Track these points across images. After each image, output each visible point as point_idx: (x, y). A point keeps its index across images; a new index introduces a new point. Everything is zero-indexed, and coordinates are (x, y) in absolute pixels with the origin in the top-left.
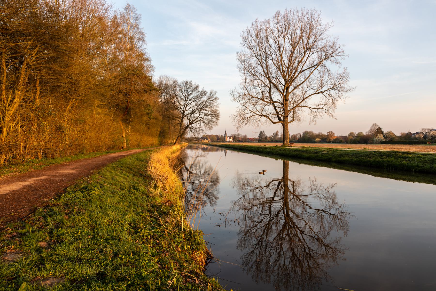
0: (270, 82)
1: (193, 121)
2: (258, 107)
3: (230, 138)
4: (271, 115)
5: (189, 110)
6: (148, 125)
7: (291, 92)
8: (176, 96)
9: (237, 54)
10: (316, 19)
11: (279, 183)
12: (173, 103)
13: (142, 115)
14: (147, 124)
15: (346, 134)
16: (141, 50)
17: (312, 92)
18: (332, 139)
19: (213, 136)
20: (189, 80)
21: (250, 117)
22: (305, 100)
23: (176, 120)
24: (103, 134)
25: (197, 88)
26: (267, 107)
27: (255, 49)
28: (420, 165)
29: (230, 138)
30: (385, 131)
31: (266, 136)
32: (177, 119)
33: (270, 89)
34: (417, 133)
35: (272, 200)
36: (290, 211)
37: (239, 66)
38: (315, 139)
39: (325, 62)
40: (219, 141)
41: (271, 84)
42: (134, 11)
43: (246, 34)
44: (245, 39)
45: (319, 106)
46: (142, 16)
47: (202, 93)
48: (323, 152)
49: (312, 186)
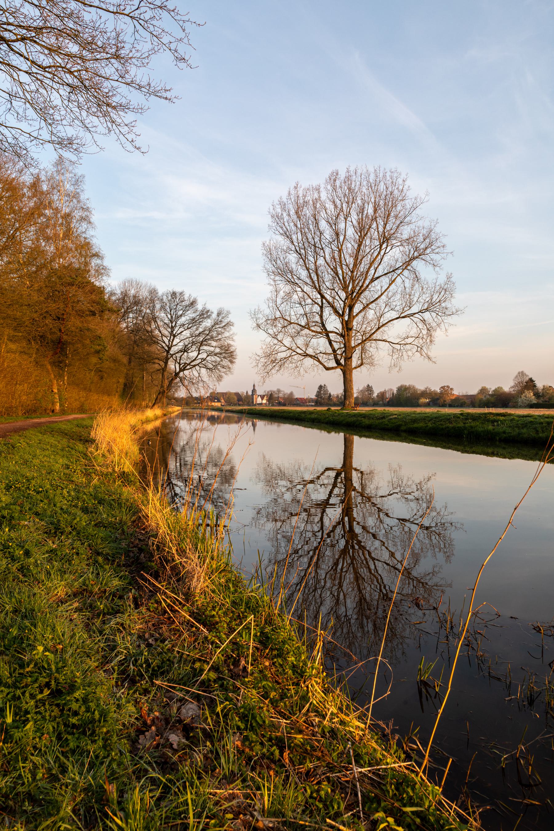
0: (323, 297)
2: (300, 341)
4: (322, 355)
5: (178, 345)
6: (101, 371)
7: (357, 315)
8: (155, 319)
9: (264, 244)
10: (401, 187)
11: (338, 475)
12: (148, 332)
13: (88, 354)
14: (99, 371)
15: (474, 391)
16: (85, 238)
17: (394, 315)
18: (448, 399)
19: (230, 394)
20: (178, 290)
21: (285, 358)
22: (381, 329)
23: (154, 363)
24: (18, 386)
25: (193, 304)
26: (314, 341)
27: (294, 237)
28: (508, 430)
30: (540, 385)
31: (330, 394)
32: (157, 361)
33: (321, 307)
35: (325, 505)
36: (355, 523)
37: (267, 266)
38: (418, 399)
39: (414, 263)
40: (241, 403)
41: (324, 301)
42: (71, 168)
43: (279, 210)
44: (277, 218)
45: (406, 340)
46: (86, 179)
47: (203, 314)
48: (392, 417)
49: (395, 479)
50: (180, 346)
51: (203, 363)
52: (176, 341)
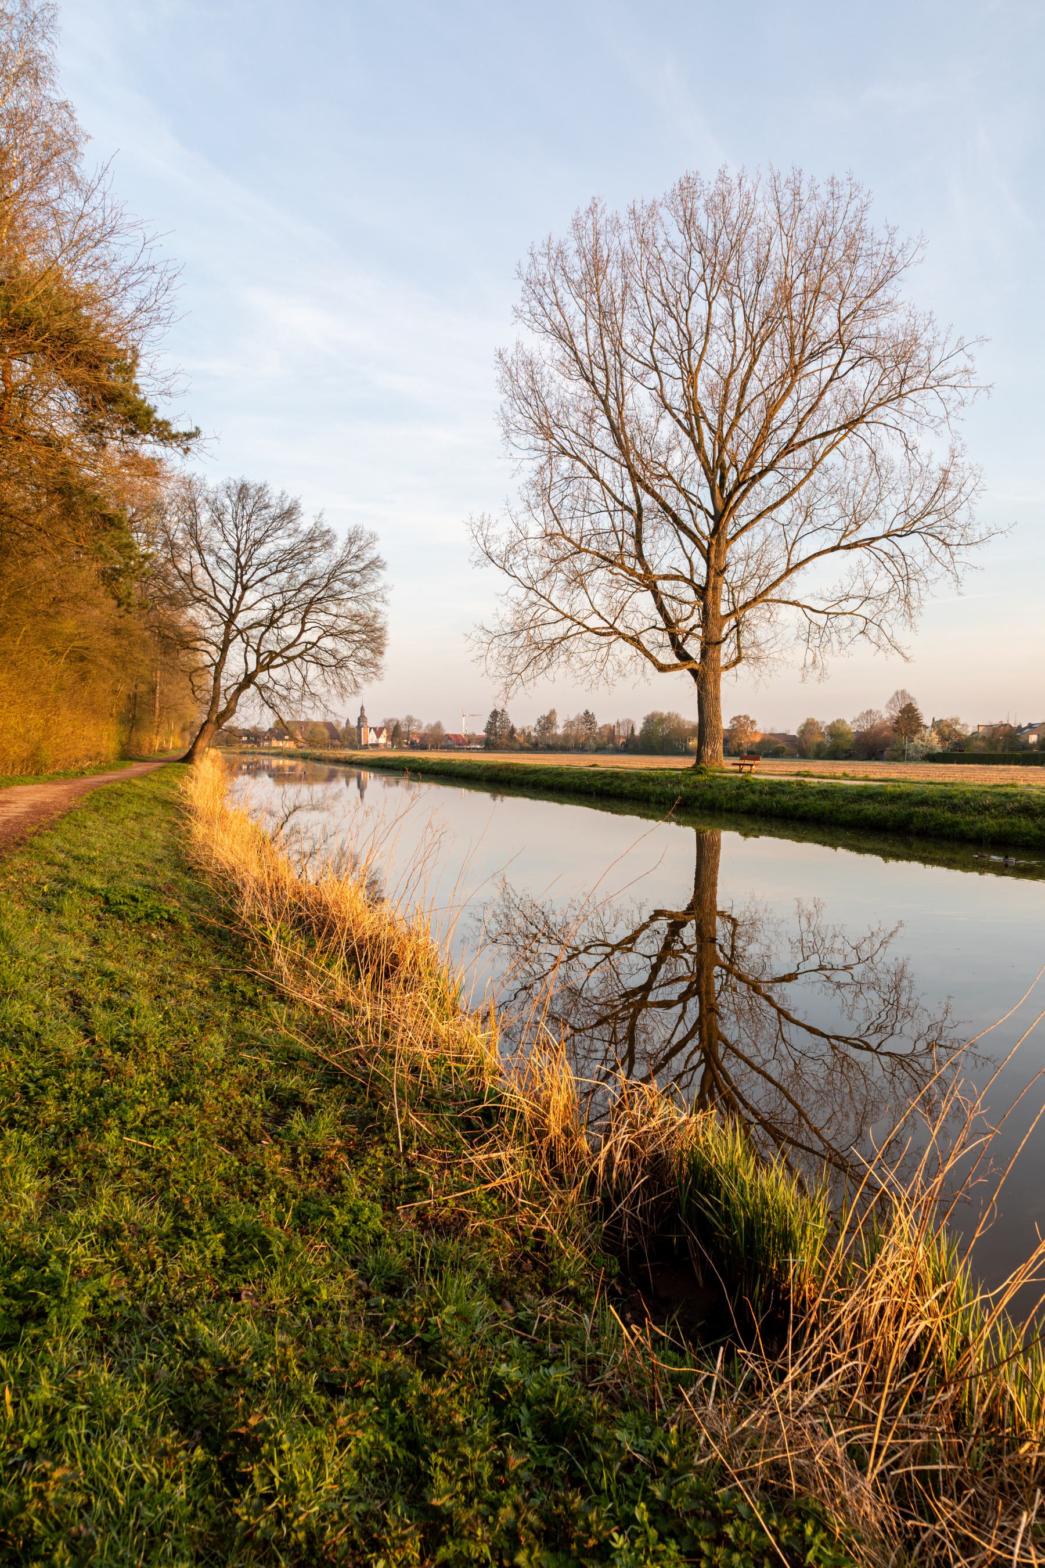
1: (273, 655)
3: (378, 732)
6: (82, 659)
9: (500, 356)
11: (676, 926)
18: (746, 741)
20: (254, 479)
25: (288, 514)
29: (378, 732)
31: (513, 730)
33: (639, 519)
34: (1030, 726)
45: (844, 604)
47: (312, 539)
50: (263, 610)
51: (310, 652)
52: (250, 597)
